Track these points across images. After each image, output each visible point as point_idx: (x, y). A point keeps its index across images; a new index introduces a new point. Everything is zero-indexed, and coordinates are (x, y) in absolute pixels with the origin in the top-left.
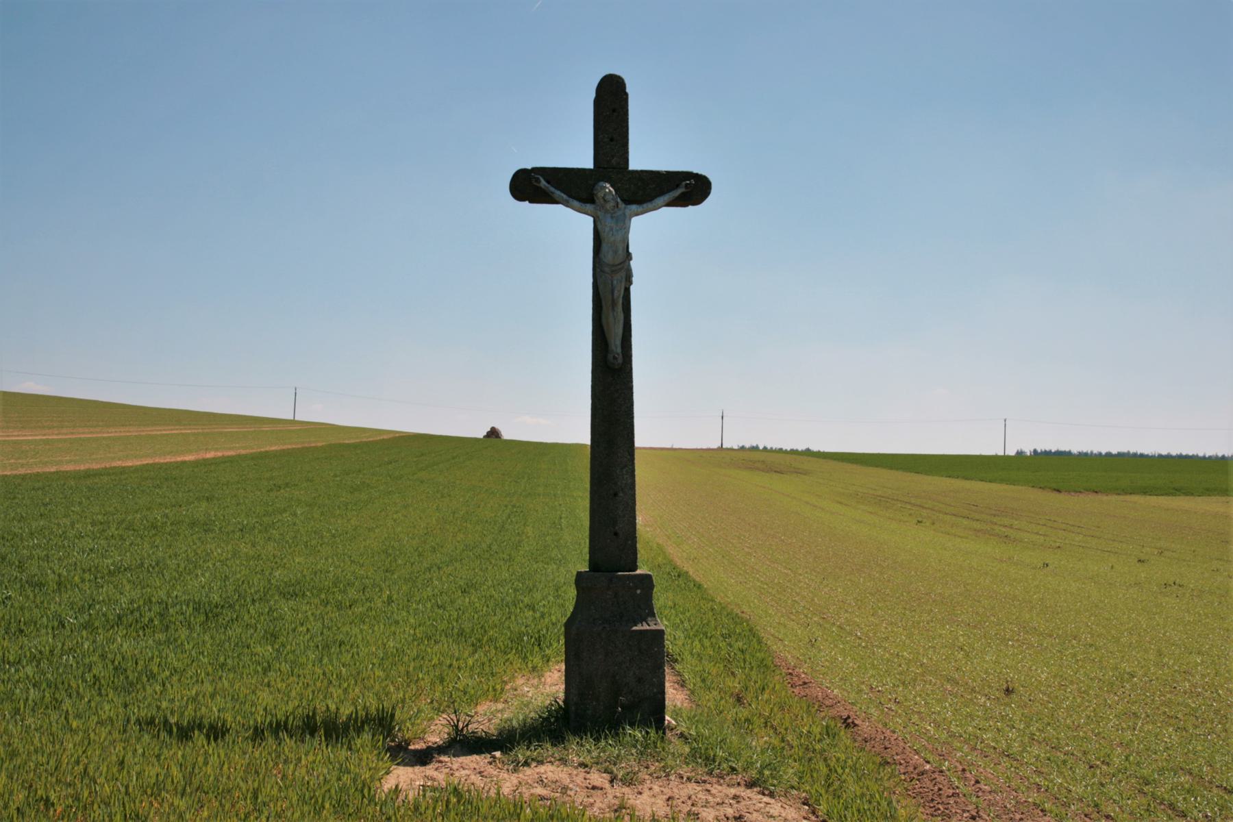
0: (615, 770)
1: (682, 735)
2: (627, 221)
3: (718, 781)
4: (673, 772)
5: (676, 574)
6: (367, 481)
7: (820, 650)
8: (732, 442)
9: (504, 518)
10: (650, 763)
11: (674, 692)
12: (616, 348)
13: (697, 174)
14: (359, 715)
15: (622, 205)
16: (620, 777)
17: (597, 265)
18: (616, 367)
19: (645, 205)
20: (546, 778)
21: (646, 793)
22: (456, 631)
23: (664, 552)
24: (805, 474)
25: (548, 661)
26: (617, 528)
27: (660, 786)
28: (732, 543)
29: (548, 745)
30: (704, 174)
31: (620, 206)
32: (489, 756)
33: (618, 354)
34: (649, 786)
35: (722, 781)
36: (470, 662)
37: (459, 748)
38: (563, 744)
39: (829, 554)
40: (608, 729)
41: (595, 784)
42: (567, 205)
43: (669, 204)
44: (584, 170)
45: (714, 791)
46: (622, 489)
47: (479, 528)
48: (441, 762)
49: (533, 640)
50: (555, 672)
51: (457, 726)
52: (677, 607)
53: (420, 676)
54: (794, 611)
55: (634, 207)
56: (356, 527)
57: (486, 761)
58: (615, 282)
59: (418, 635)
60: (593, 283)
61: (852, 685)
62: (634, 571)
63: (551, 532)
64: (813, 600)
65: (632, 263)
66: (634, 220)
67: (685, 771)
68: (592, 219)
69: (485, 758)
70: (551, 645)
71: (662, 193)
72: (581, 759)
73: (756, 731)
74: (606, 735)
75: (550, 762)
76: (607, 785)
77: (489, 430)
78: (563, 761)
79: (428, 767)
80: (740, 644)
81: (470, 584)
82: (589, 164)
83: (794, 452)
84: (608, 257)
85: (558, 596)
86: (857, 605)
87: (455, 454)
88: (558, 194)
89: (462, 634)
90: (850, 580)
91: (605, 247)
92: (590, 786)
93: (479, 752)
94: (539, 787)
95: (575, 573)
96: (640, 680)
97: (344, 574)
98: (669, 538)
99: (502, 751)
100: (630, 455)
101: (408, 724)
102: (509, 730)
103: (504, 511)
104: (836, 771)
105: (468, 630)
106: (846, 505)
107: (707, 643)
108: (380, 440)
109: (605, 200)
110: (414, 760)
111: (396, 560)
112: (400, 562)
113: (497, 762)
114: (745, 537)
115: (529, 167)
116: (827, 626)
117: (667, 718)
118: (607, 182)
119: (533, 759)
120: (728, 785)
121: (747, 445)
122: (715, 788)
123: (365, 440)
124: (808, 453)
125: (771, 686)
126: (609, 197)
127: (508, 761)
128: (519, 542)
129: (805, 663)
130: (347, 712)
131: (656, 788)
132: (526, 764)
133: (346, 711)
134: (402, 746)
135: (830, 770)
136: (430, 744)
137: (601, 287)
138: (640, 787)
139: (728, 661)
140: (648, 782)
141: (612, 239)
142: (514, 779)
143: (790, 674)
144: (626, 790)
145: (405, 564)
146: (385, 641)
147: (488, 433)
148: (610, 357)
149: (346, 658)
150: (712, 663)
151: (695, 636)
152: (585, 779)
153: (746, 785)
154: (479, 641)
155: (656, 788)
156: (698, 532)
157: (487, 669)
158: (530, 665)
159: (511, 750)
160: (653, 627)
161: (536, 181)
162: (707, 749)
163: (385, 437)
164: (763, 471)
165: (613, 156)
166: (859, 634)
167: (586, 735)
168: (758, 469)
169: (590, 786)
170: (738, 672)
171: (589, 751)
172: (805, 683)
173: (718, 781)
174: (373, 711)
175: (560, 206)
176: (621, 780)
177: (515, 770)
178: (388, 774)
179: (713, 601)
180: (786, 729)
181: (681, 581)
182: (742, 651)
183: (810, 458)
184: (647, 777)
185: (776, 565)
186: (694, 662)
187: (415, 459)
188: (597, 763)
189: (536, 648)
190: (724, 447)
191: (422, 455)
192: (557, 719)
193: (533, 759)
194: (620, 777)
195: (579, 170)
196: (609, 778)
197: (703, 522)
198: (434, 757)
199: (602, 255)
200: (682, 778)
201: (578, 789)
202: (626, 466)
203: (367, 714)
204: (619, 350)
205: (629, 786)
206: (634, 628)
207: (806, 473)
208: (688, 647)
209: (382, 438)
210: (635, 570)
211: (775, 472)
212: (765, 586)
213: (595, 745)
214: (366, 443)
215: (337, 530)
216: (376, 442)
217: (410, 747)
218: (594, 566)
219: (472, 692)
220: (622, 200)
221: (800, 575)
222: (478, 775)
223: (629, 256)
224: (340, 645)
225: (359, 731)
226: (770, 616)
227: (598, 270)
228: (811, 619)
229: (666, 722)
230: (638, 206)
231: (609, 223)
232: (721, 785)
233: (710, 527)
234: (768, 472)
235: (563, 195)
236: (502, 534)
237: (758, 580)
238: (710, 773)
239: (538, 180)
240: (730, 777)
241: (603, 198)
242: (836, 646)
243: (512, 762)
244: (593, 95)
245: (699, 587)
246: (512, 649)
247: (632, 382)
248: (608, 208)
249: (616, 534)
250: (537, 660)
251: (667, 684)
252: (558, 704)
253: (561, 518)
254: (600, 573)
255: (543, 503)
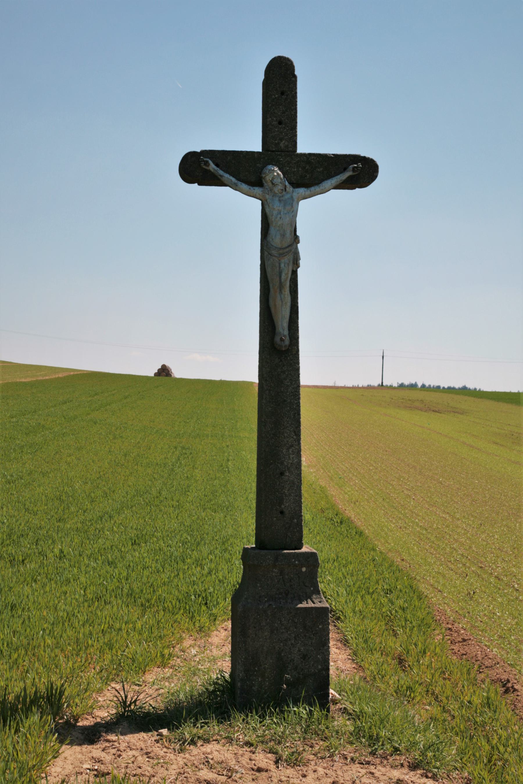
0: (280, 749)
1: (345, 711)
2: (294, 203)
3: (382, 762)
4: (337, 752)
5: (339, 521)
6: (42, 422)
7: (478, 603)
8: (392, 380)
9: (174, 460)
10: (314, 742)
11: (337, 651)
12: (283, 330)
13: (364, 158)
14: (28, 692)
15: (289, 188)
16: (284, 757)
17: (265, 248)
18: (284, 349)
19: (313, 189)
20: (212, 759)
21: (311, 776)
22: (125, 591)
23: (327, 496)
24: (462, 414)
25: (215, 620)
26: (283, 506)
27: (325, 768)
28: (392, 485)
29: (215, 723)
30: (371, 157)
31: (287, 189)
32: (156, 733)
33: (285, 336)
34: (313, 768)
35: (385, 762)
36: (139, 625)
37: (126, 725)
38: (230, 721)
39: (485, 497)
40: (272, 706)
41: (260, 765)
42: (235, 187)
43: (338, 187)
44: (253, 153)
45: (377, 774)
46: (288, 469)
47: (149, 471)
48: (108, 741)
49: (200, 599)
50: (222, 631)
51: (125, 702)
52: (340, 559)
53: (90, 642)
54: (452, 559)
55: (302, 191)
56: (31, 472)
57: (153, 739)
58: (282, 265)
59: (89, 596)
60: (261, 265)
61: (510, 644)
62: (300, 549)
63: (218, 475)
64: (470, 547)
65: (299, 246)
66: (303, 204)
67: (349, 751)
68: (260, 202)
69: (152, 736)
70: (218, 603)
71: (330, 177)
72: (246, 738)
73: (418, 698)
74: (271, 712)
75: (216, 740)
76: (272, 767)
77: (160, 367)
78: (230, 740)
79: (95, 747)
80: (400, 602)
81: (140, 536)
82: (256, 146)
83: (451, 390)
84: (276, 240)
85: (226, 550)
86: (514, 553)
87: (127, 394)
88: (227, 177)
89: (131, 595)
90: (507, 526)
91: (272, 231)
92: (255, 768)
93: (146, 730)
94: (205, 770)
95: (242, 548)
96: (304, 657)
97: (18, 523)
98: (331, 479)
99: (169, 729)
100: (296, 435)
101: (77, 700)
102: (176, 704)
103: (173, 452)
104: (498, 749)
105: (138, 591)
106: (502, 446)
107: (368, 598)
108: (55, 378)
109: (273, 184)
110: (82, 738)
111: (68, 508)
112: (72, 509)
113: (164, 740)
114: (404, 479)
115: (198, 150)
116: (486, 576)
117: (331, 691)
118: (275, 165)
119: (199, 738)
120: (392, 767)
121: (407, 383)
122: (379, 770)
123: (40, 378)
124: (464, 391)
125: (432, 648)
126: (277, 181)
127: (175, 739)
128: (188, 486)
129: (465, 617)
130: (17, 690)
131: (321, 771)
132: (193, 742)
133: (17, 688)
134: (71, 724)
135: (493, 748)
136: (99, 720)
137: (269, 270)
138: (305, 769)
139: (389, 620)
140: (313, 763)
141: (280, 223)
142: (180, 759)
143: (450, 629)
144: (290, 771)
145: (78, 511)
146: (56, 602)
147: (159, 370)
148: (277, 339)
149: (17, 624)
150: (375, 621)
151: (358, 592)
152: (250, 760)
153: (409, 766)
154: (148, 601)
155: (321, 771)
156: (359, 473)
157: (156, 633)
158: (197, 625)
159: (178, 728)
160: (318, 605)
161: (205, 164)
162: (370, 728)
163: (60, 375)
164: (421, 410)
165: (281, 140)
166: (516, 586)
167: (251, 713)
168: (417, 408)
169: (255, 768)
170: (400, 631)
171: (254, 729)
172: (464, 640)
173: (382, 762)
174: (43, 689)
175: (228, 188)
176: (286, 761)
177: (181, 751)
178: (56, 758)
179: (374, 550)
180: (447, 698)
181: (343, 528)
182: (403, 609)
183: (466, 398)
184: (312, 757)
185: (434, 509)
186: (357, 620)
187: (89, 399)
188: (262, 742)
189: (204, 608)
190: (384, 384)
191: (96, 394)
192: (223, 692)
193: (199, 738)
194: (284, 757)
195: (247, 152)
196: (274, 759)
197: (364, 462)
198: (102, 736)
199: (269, 239)
200: (346, 758)
201: (244, 772)
202: (292, 446)
203: (36, 693)
204: (286, 332)
205: (293, 767)
206: (300, 606)
207: (462, 412)
208: (350, 605)
209: (57, 376)
210: (300, 548)
211: (433, 411)
212: (424, 532)
213: (261, 722)
214: (42, 381)
215: (12, 476)
216: (51, 381)
217: (78, 724)
218: (261, 544)
219: (141, 659)
220: (289, 183)
221: (458, 519)
222: (145, 756)
223: (296, 239)
224: (12, 609)
225: (27, 711)
226: (430, 564)
227: (266, 253)
228: (469, 568)
229: (331, 695)
230: (305, 189)
231: (277, 206)
232: (385, 766)
233: (371, 468)
234: (426, 411)
235: (231, 178)
236: (171, 477)
237: (417, 525)
238: (373, 753)
239: (207, 164)
240: (394, 757)
241: (271, 182)
242: (495, 600)
243: (179, 740)
244: (262, 77)
245: (361, 534)
246: (180, 609)
247: (298, 363)
248: (276, 191)
249: (282, 512)
250: (204, 620)
251: (331, 643)
252: (224, 677)
253: (228, 460)
254: (266, 551)
255: (212, 444)
